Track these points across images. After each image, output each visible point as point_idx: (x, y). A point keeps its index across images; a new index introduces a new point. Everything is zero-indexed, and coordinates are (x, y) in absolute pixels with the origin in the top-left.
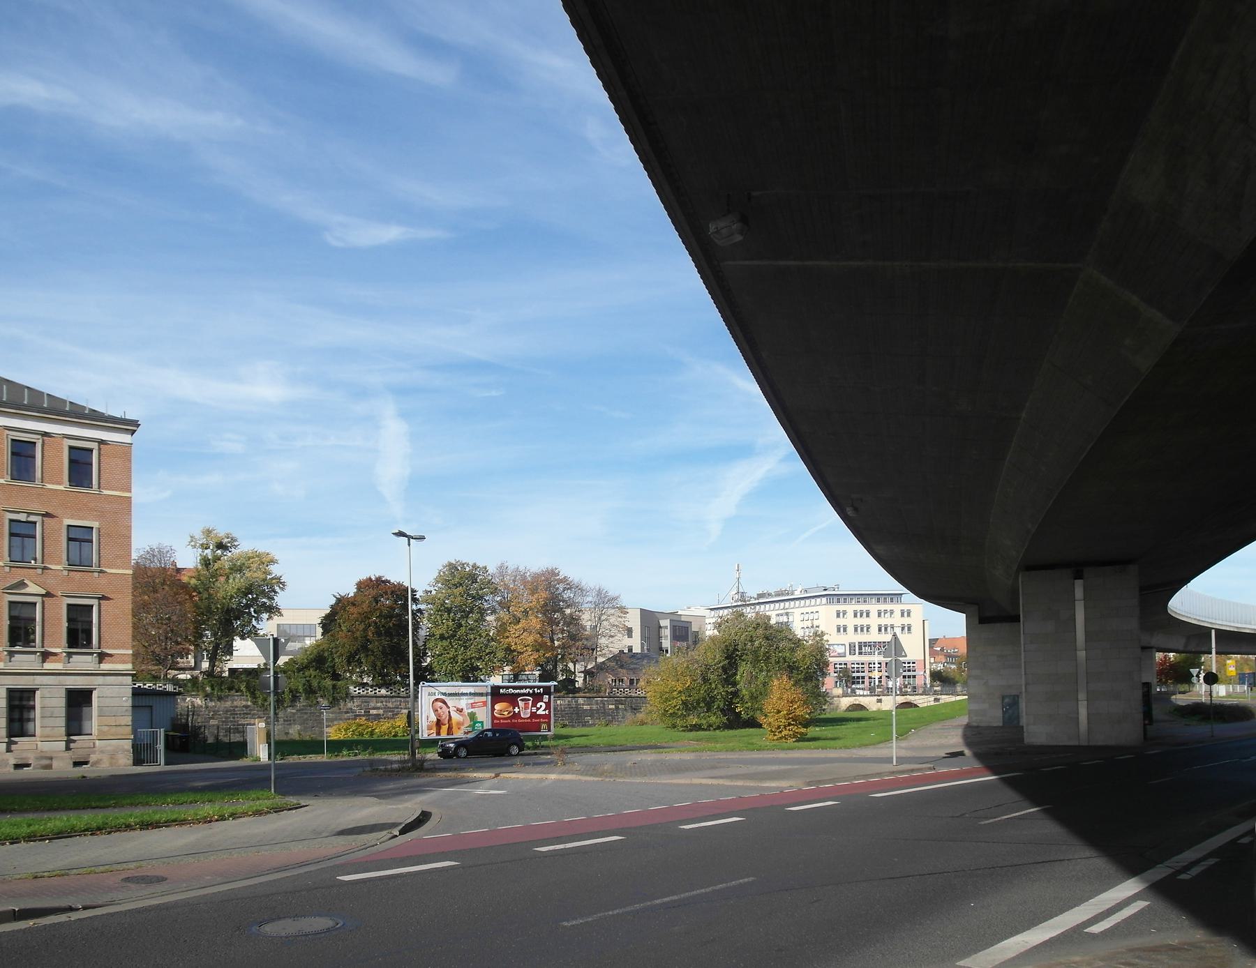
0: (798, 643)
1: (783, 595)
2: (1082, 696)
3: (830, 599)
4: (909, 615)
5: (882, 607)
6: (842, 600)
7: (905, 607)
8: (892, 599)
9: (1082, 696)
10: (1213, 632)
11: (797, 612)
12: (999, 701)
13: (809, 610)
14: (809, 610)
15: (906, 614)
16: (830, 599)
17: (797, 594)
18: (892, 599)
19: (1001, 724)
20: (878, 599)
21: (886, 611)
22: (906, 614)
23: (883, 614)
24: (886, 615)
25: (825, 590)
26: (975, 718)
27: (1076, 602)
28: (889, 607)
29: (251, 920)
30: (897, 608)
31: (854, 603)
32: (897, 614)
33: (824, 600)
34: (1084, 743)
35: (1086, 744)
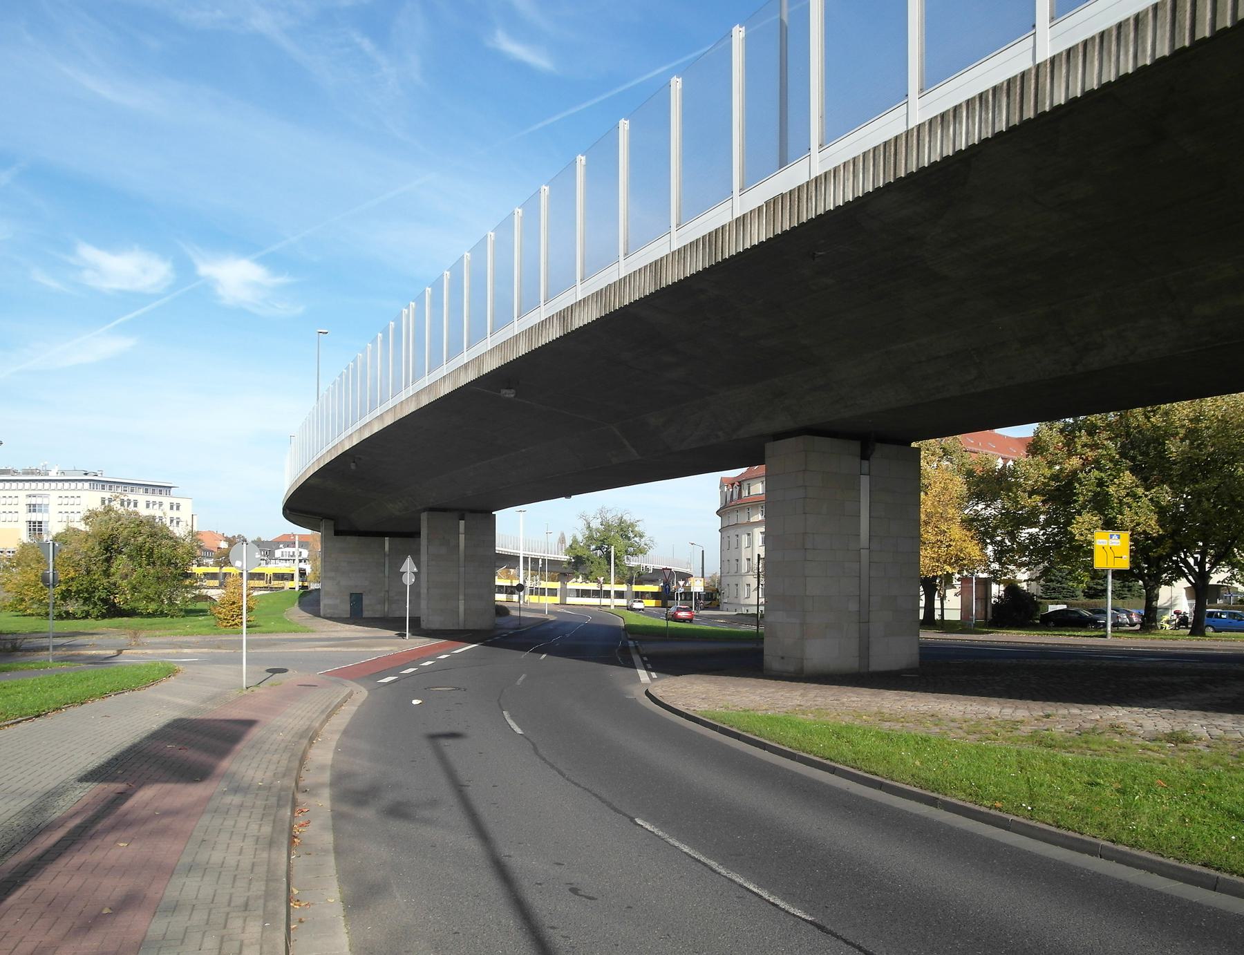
0: (176, 542)
1: (33, 473)
2: (461, 597)
3: (94, 485)
4: (178, 508)
5: (152, 498)
6: (107, 487)
7: (175, 501)
8: (160, 491)
9: (461, 597)
10: (540, 560)
11: (54, 495)
12: (348, 598)
13: (69, 494)
14: (69, 494)
15: (175, 507)
16: (94, 485)
17: (53, 475)
18: (103, 486)
19: (349, 616)
20: (147, 490)
21: (154, 503)
22: (175, 507)
23: (151, 505)
24: (155, 507)
25: (86, 474)
26: (328, 611)
27: (960, 608)
28: (157, 499)
29: (973, 723)
30: (166, 501)
31: (141, 493)
32: (166, 507)
33: (87, 485)
34: (461, 628)
35: (463, 629)
